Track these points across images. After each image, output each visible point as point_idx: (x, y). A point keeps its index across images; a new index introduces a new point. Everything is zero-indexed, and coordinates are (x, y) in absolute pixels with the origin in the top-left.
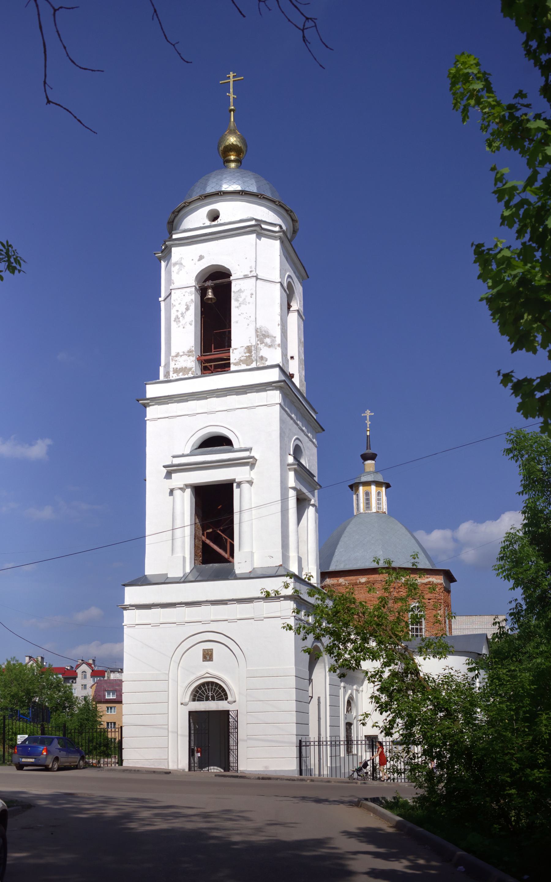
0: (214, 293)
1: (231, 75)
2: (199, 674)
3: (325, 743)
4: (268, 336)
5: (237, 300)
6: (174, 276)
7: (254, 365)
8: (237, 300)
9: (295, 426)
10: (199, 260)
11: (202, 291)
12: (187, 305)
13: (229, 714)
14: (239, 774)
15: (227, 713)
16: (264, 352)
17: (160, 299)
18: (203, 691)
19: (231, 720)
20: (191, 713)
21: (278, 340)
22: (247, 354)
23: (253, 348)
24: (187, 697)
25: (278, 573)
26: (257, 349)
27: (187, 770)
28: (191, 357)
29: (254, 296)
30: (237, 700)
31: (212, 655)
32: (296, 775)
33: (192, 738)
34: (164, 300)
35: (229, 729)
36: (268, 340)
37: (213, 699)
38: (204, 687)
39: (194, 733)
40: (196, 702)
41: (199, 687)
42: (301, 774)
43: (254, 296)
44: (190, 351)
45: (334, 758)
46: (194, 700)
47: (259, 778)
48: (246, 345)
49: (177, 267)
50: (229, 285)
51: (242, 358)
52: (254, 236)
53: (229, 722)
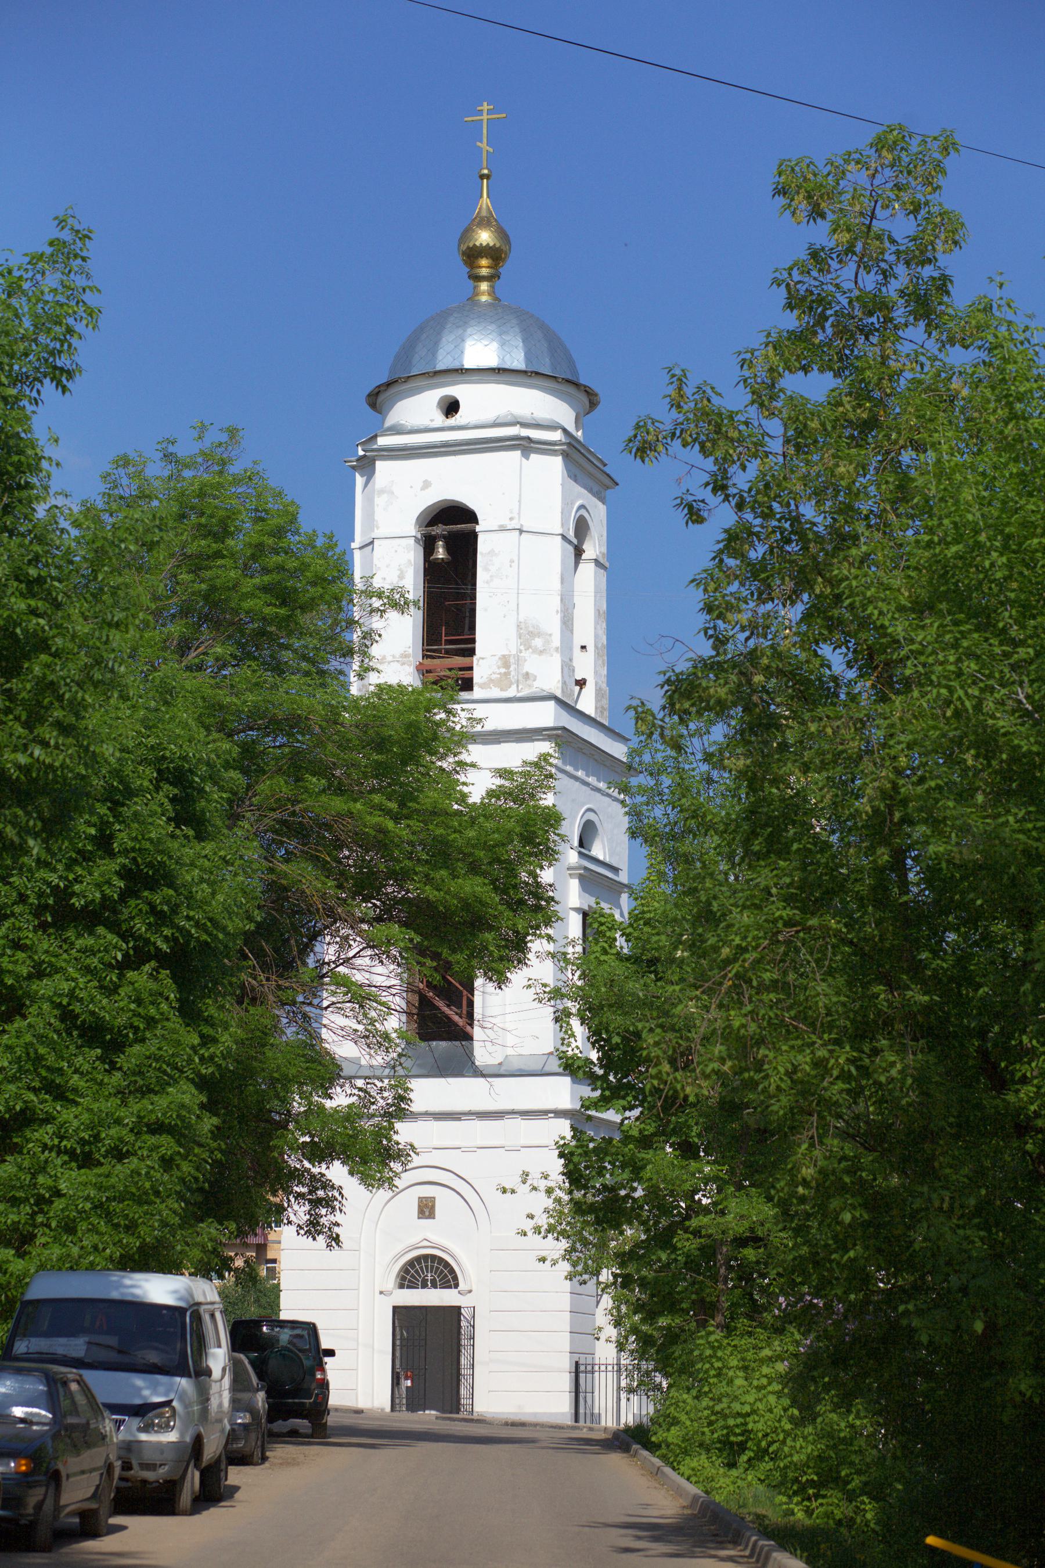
0: (448, 549)
1: (485, 107)
2: (414, 1240)
3: (603, 1368)
4: (539, 635)
5: (486, 569)
6: (379, 515)
7: (511, 692)
8: (486, 569)
9: (584, 788)
10: (423, 489)
11: (428, 544)
12: (401, 570)
13: (460, 1314)
14: (475, 1416)
15: (457, 1310)
16: (532, 664)
17: (353, 545)
18: (417, 1272)
19: (463, 1323)
20: (396, 1310)
21: (556, 641)
22: (503, 670)
23: (512, 660)
24: (390, 1281)
25: (547, 1069)
26: (519, 661)
27: (388, 1409)
28: (406, 667)
29: (515, 565)
30: (474, 1289)
31: (433, 1208)
32: (569, 1421)
33: (398, 1354)
34: (360, 548)
35: (459, 1340)
36: (538, 642)
37: (434, 1286)
38: (419, 1263)
39: (401, 1346)
40: (405, 1291)
41: (411, 1263)
42: (577, 1420)
43: (515, 565)
44: (404, 655)
45: (589, 1389)
46: (401, 1286)
47: (506, 1424)
48: (500, 653)
49: (385, 497)
50: (473, 537)
51: (494, 677)
52: (518, 453)
53: (460, 1327)
